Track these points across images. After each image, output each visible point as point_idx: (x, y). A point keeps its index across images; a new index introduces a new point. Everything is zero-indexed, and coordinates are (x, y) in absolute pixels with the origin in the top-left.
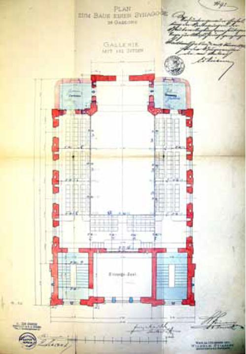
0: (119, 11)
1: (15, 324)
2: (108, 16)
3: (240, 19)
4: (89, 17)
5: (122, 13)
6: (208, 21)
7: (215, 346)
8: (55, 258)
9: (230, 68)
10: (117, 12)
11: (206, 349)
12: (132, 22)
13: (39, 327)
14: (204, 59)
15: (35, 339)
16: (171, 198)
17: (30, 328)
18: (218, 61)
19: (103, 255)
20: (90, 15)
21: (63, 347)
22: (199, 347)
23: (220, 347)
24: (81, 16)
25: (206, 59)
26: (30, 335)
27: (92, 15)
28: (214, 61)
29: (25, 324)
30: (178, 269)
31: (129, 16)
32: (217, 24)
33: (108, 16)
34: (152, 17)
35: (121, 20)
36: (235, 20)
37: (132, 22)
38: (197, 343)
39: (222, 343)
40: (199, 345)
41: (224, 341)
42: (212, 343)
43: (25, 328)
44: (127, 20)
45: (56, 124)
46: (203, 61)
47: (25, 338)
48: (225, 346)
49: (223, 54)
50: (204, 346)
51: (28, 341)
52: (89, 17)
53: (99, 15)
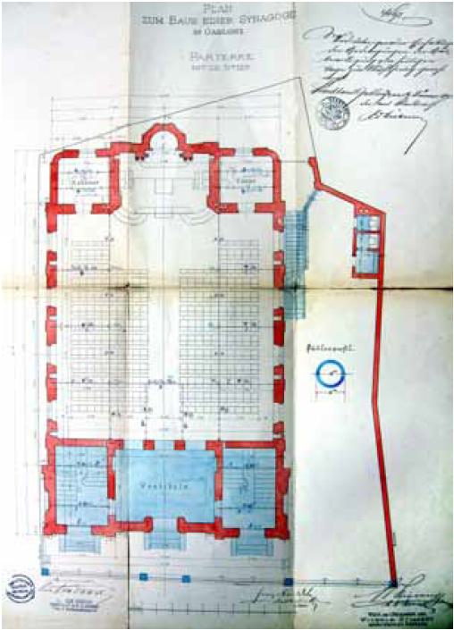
2: (194, 21)
4: (162, 23)
5: (215, 16)
6: (380, 43)
7: (401, 620)
8: (52, 455)
9: (415, 140)
12: (235, 32)
14: (379, 114)
15: (31, 583)
16: (188, 356)
17: (79, 608)
20: (162, 19)
22: (375, 622)
23: (409, 621)
24: (148, 20)
27: (166, 20)
28: (395, 117)
30: (260, 481)
31: (229, 20)
32: (393, 48)
34: (268, 23)
37: (235, 32)
40: (374, 618)
44: (227, 27)
45: (52, 228)
49: (425, 105)
52: (162, 23)
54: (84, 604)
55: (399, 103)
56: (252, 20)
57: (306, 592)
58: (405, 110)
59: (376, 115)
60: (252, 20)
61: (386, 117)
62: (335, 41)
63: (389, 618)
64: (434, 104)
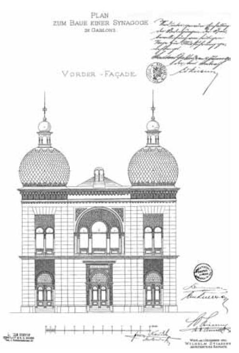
0: (97, 17)
1: (7, 336)
2: (85, 23)
3: (219, 23)
10: (95, 19)
11: (201, 347)
12: (110, 30)
13: (33, 338)
14: (186, 70)
17: (22, 339)
18: (202, 72)
19: (161, 237)
21: (205, 296)
24: (57, 23)
25: (188, 69)
26: (205, 265)
27: (68, 23)
28: (198, 72)
29: (17, 335)
31: (107, 23)
33: (85, 23)
35: (97, 27)
36: (214, 25)
37: (110, 30)
38: (191, 340)
39: (218, 340)
40: (194, 343)
41: (220, 339)
42: (207, 340)
43: (16, 339)
44: (105, 27)
46: (185, 72)
47: (200, 270)
48: (222, 343)
50: (199, 344)
51: (204, 273)
53: (75, 22)
54: (25, 337)
55: (202, 64)
56: (121, 23)
57: (165, 333)
58: (203, 67)
59: (184, 70)
60: (121, 23)
61: (191, 71)
62: (162, 24)
63: (203, 343)
64: (221, 63)
